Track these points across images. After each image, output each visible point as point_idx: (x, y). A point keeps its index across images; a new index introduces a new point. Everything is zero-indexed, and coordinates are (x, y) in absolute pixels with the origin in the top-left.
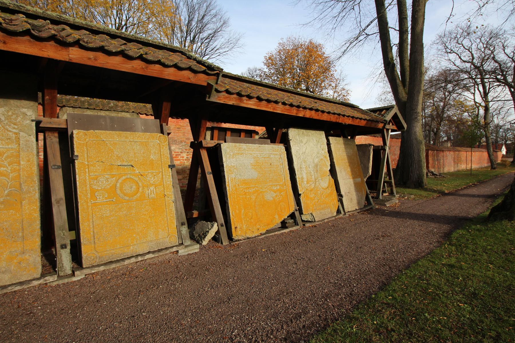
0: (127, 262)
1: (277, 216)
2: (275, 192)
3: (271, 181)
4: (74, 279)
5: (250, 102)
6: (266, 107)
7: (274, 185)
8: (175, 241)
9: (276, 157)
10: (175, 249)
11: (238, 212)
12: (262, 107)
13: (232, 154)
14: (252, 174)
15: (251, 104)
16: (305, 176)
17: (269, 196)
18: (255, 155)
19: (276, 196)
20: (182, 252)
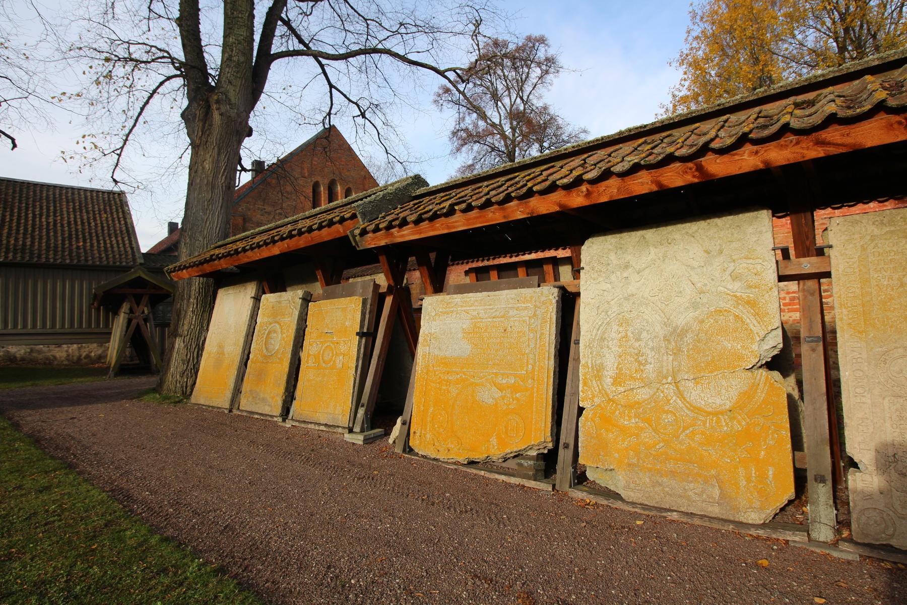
0: (310, 426)
1: (494, 441)
2: (501, 390)
3: (498, 365)
4: (835, 554)
5: (405, 232)
6: (433, 230)
7: (503, 374)
8: (344, 419)
9: (525, 313)
10: (340, 430)
11: (422, 408)
12: (426, 232)
13: (433, 314)
14: (460, 348)
15: (408, 235)
16: (610, 363)
17: (488, 395)
18: (475, 313)
19: (503, 398)
20: (348, 437)
